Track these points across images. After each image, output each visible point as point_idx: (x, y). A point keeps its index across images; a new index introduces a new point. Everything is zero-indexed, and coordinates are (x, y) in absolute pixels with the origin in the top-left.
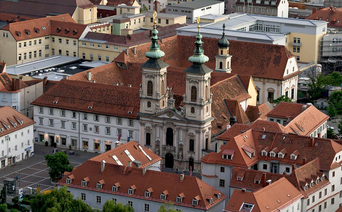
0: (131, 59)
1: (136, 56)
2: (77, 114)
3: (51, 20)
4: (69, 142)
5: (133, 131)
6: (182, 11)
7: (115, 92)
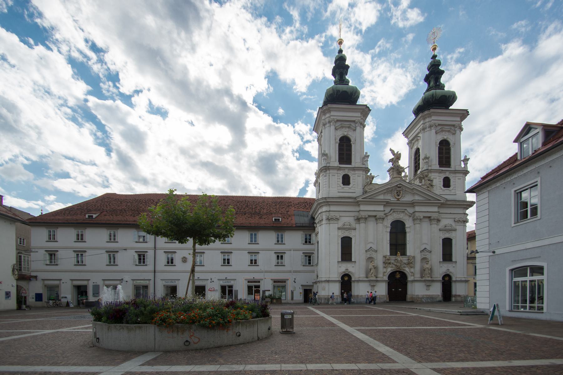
5: (285, 253)
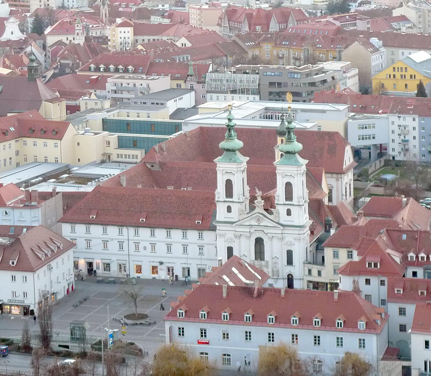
0: (162, 158)
1: (165, 153)
2: (125, 229)
3: (18, 119)
4: (114, 268)
5: (204, 246)
6: (152, 103)
7: (173, 198)
